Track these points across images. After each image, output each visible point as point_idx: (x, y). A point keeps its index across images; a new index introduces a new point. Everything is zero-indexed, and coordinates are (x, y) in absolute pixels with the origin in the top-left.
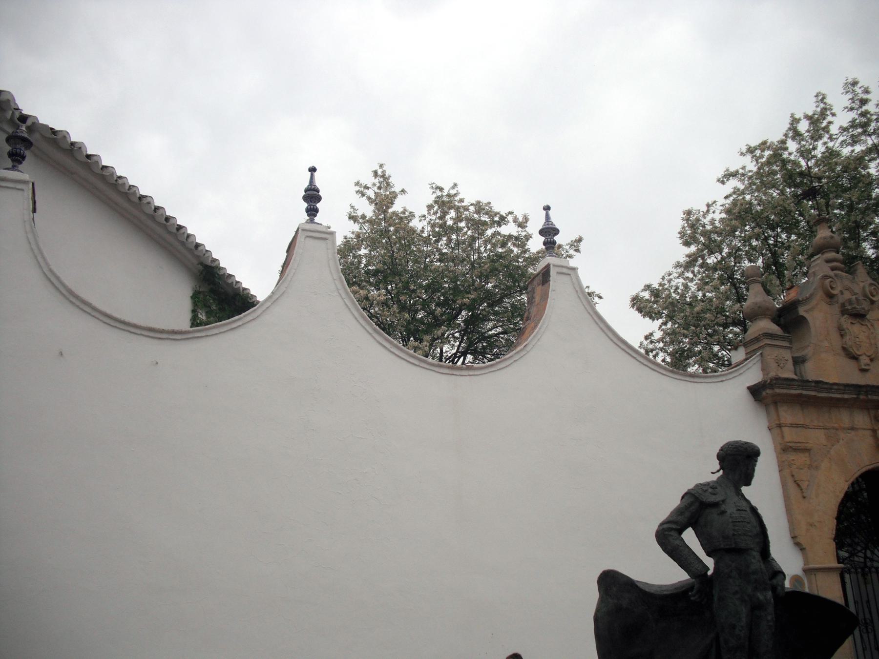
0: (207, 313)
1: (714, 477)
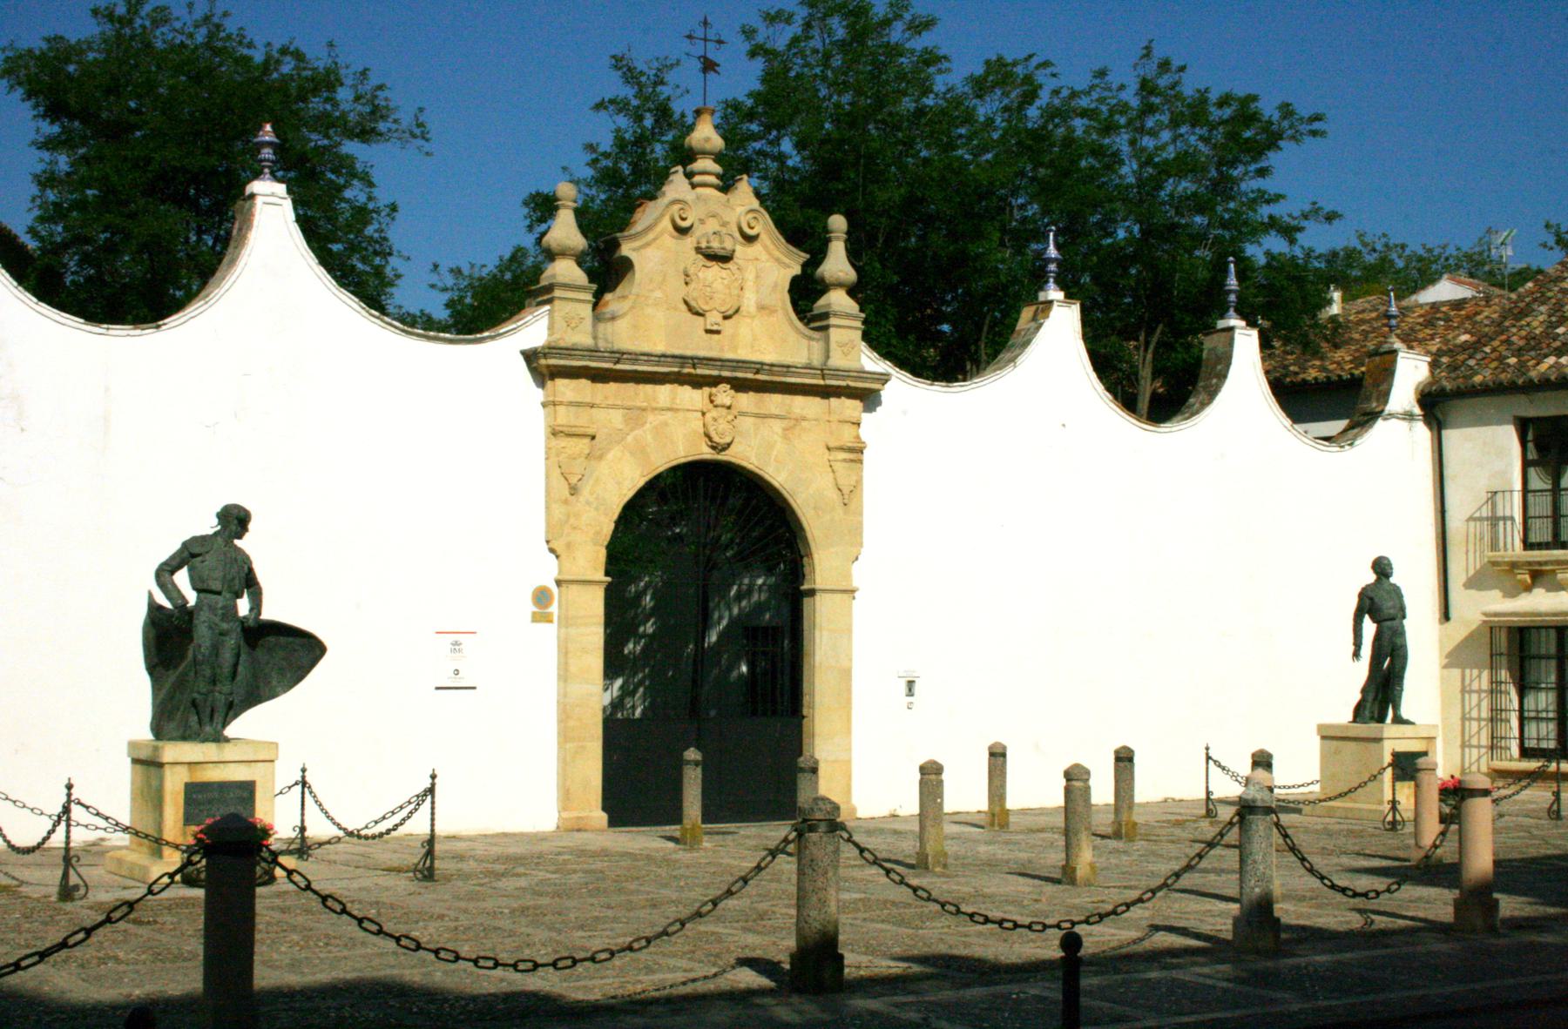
0: (844, 41)
1: (211, 532)
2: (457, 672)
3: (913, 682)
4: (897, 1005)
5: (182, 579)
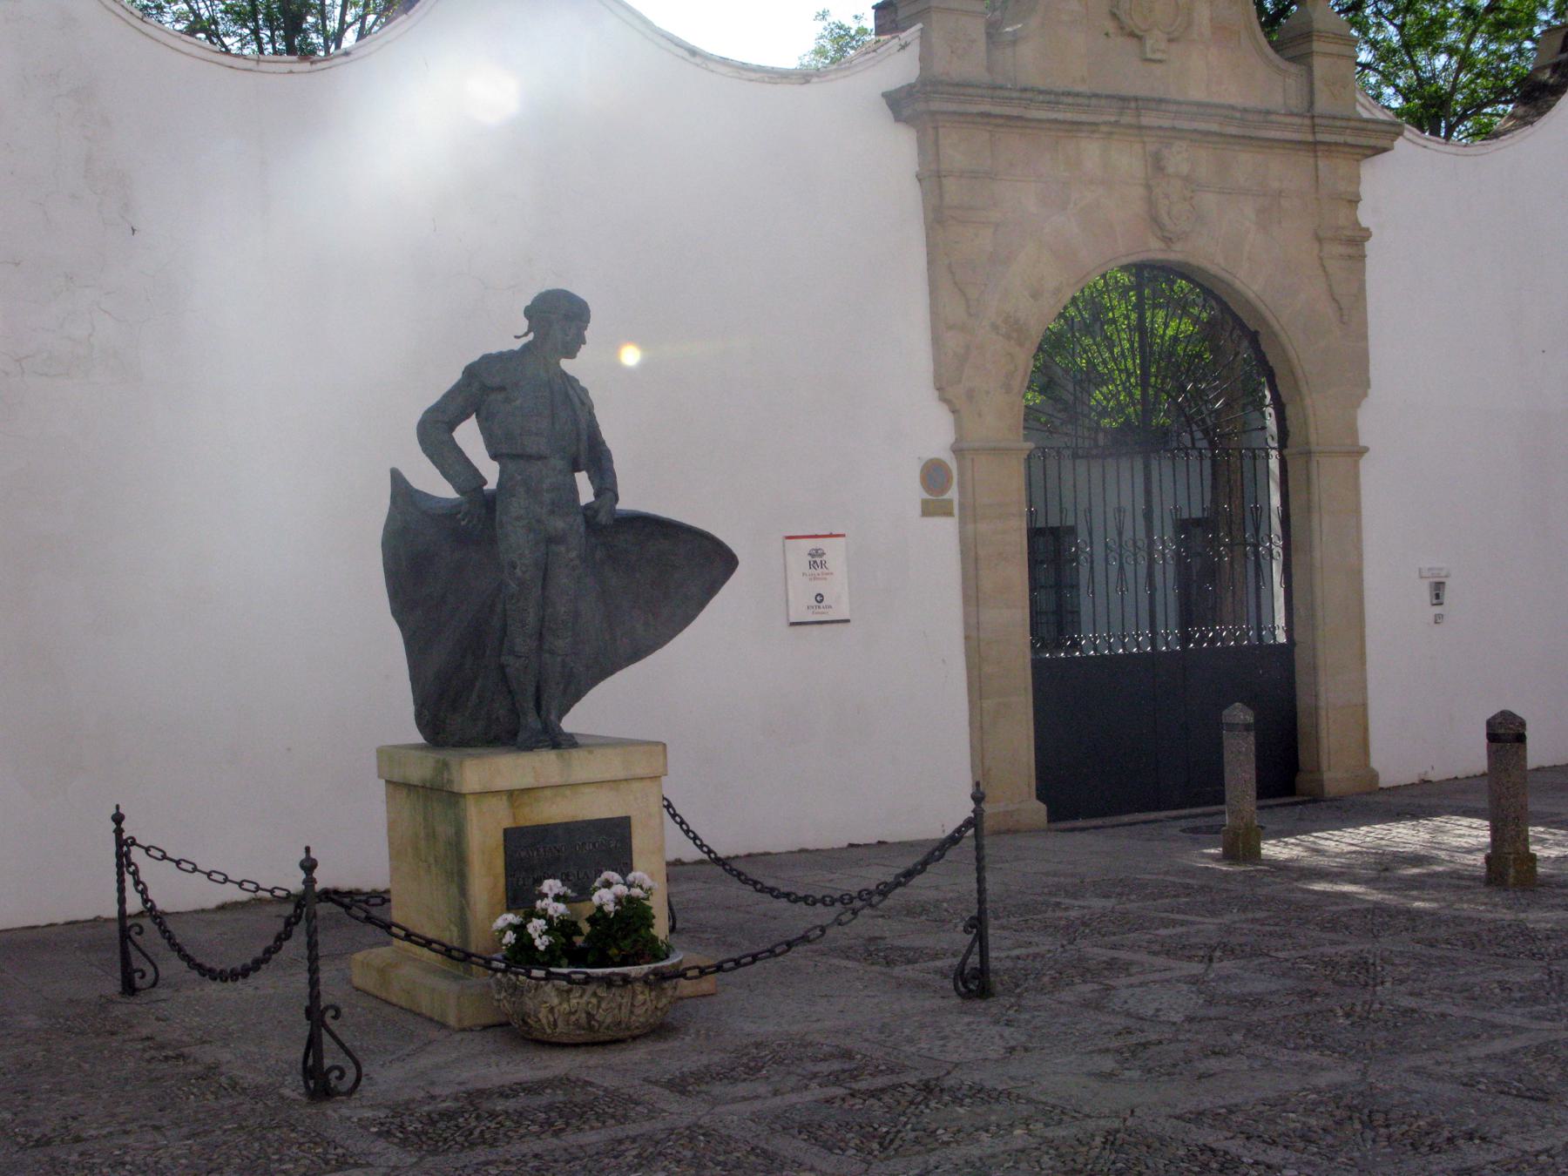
1: (517, 345)
2: (820, 598)
3: (1443, 583)
4: (1170, 969)
5: (469, 436)
